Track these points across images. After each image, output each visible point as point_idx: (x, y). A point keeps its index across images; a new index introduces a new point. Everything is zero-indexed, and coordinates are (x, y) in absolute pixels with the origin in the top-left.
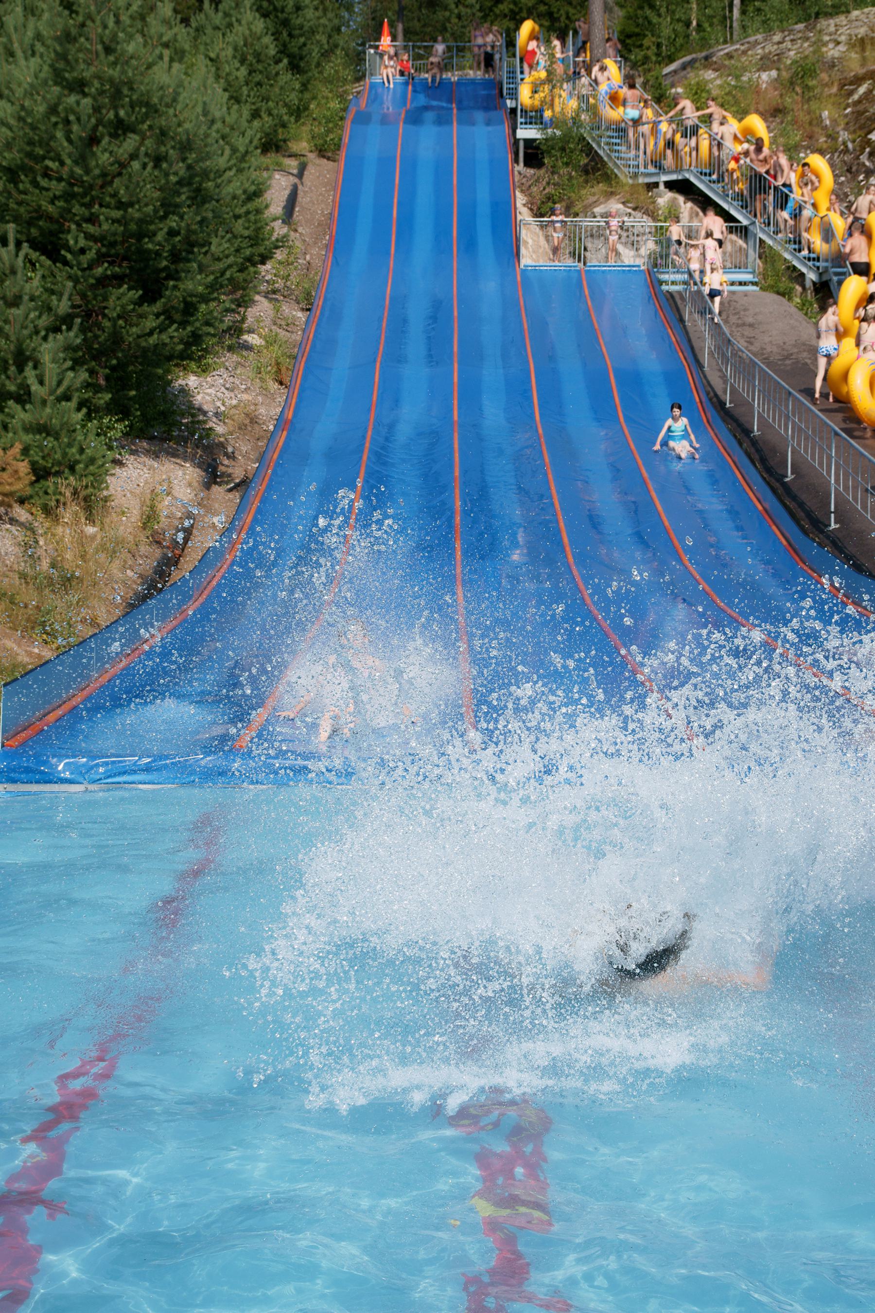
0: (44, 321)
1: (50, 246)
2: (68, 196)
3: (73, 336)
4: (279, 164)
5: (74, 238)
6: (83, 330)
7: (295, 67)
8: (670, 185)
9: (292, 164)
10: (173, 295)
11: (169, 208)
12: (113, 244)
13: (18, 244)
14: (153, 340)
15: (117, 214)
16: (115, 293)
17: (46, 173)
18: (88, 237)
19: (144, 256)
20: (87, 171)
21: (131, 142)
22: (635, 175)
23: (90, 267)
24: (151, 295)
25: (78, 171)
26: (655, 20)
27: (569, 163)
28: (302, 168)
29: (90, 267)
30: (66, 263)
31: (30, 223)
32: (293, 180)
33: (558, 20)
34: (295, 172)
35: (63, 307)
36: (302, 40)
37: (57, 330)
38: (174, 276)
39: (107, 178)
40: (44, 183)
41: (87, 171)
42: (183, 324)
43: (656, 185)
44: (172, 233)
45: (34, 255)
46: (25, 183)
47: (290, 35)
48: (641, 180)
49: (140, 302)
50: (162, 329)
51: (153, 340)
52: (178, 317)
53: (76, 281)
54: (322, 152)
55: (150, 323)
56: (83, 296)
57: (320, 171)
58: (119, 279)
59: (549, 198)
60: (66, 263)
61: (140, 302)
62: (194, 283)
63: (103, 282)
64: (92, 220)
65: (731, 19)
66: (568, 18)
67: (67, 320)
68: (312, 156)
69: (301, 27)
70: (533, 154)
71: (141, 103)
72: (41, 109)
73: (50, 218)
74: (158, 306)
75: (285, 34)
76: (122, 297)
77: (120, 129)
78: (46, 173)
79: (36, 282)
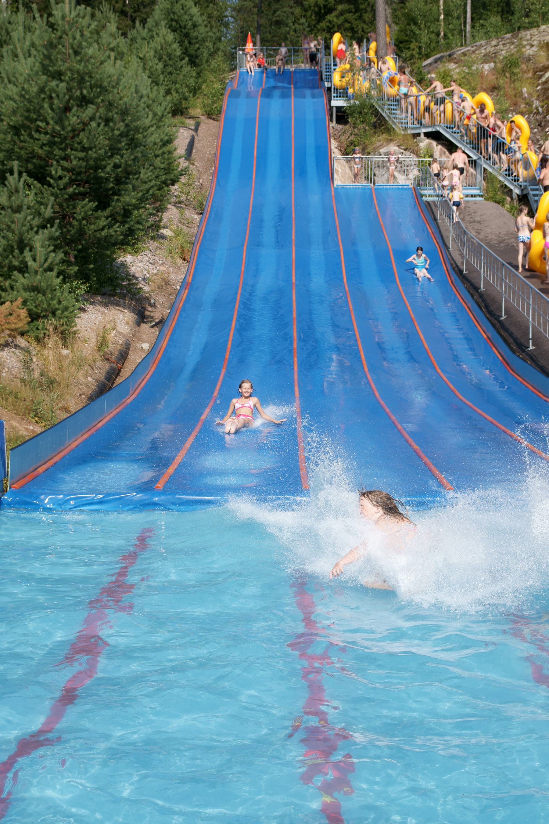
0: (37, 221)
1: (40, 175)
2: (51, 144)
4: (183, 123)
5: (55, 170)
6: (61, 227)
7: (193, 62)
10: (117, 205)
11: (114, 150)
12: (79, 173)
13: (20, 174)
15: (82, 155)
18: (64, 169)
19: (99, 181)
20: (63, 128)
21: (90, 110)
22: (406, 129)
23: (65, 188)
24: (103, 205)
25: (58, 128)
26: (418, 32)
27: (363, 121)
28: (197, 125)
29: (65, 188)
30: (50, 185)
31: (27, 161)
34: (193, 127)
35: (48, 212)
36: (197, 46)
37: (44, 227)
38: (117, 193)
39: (75, 133)
40: (36, 135)
41: (63, 128)
42: (123, 223)
43: (419, 135)
44: (116, 166)
45: (30, 180)
46: (24, 135)
47: (190, 43)
48: (409, 132)
49: (96, 209)
51: (104, 233)
52: (119, 218)
53: (56, 196)
55: (103, 222)
56: (61, 206)
57: (208, 127)
58: (83, 195)
60: (50, 185)
61: (96, 209)
62: (130, 198)
63: (73, 197)
64: (66, 158)
66: (363, 31)
67: (51, 221)
68: (203, 118)
69: (197, 38)
71: (97, 86)
73: (40, 158)
74: (107, 212)
75: (186, 42)
76: (85, 206)
77: (84, 101)
79: (31, 197)
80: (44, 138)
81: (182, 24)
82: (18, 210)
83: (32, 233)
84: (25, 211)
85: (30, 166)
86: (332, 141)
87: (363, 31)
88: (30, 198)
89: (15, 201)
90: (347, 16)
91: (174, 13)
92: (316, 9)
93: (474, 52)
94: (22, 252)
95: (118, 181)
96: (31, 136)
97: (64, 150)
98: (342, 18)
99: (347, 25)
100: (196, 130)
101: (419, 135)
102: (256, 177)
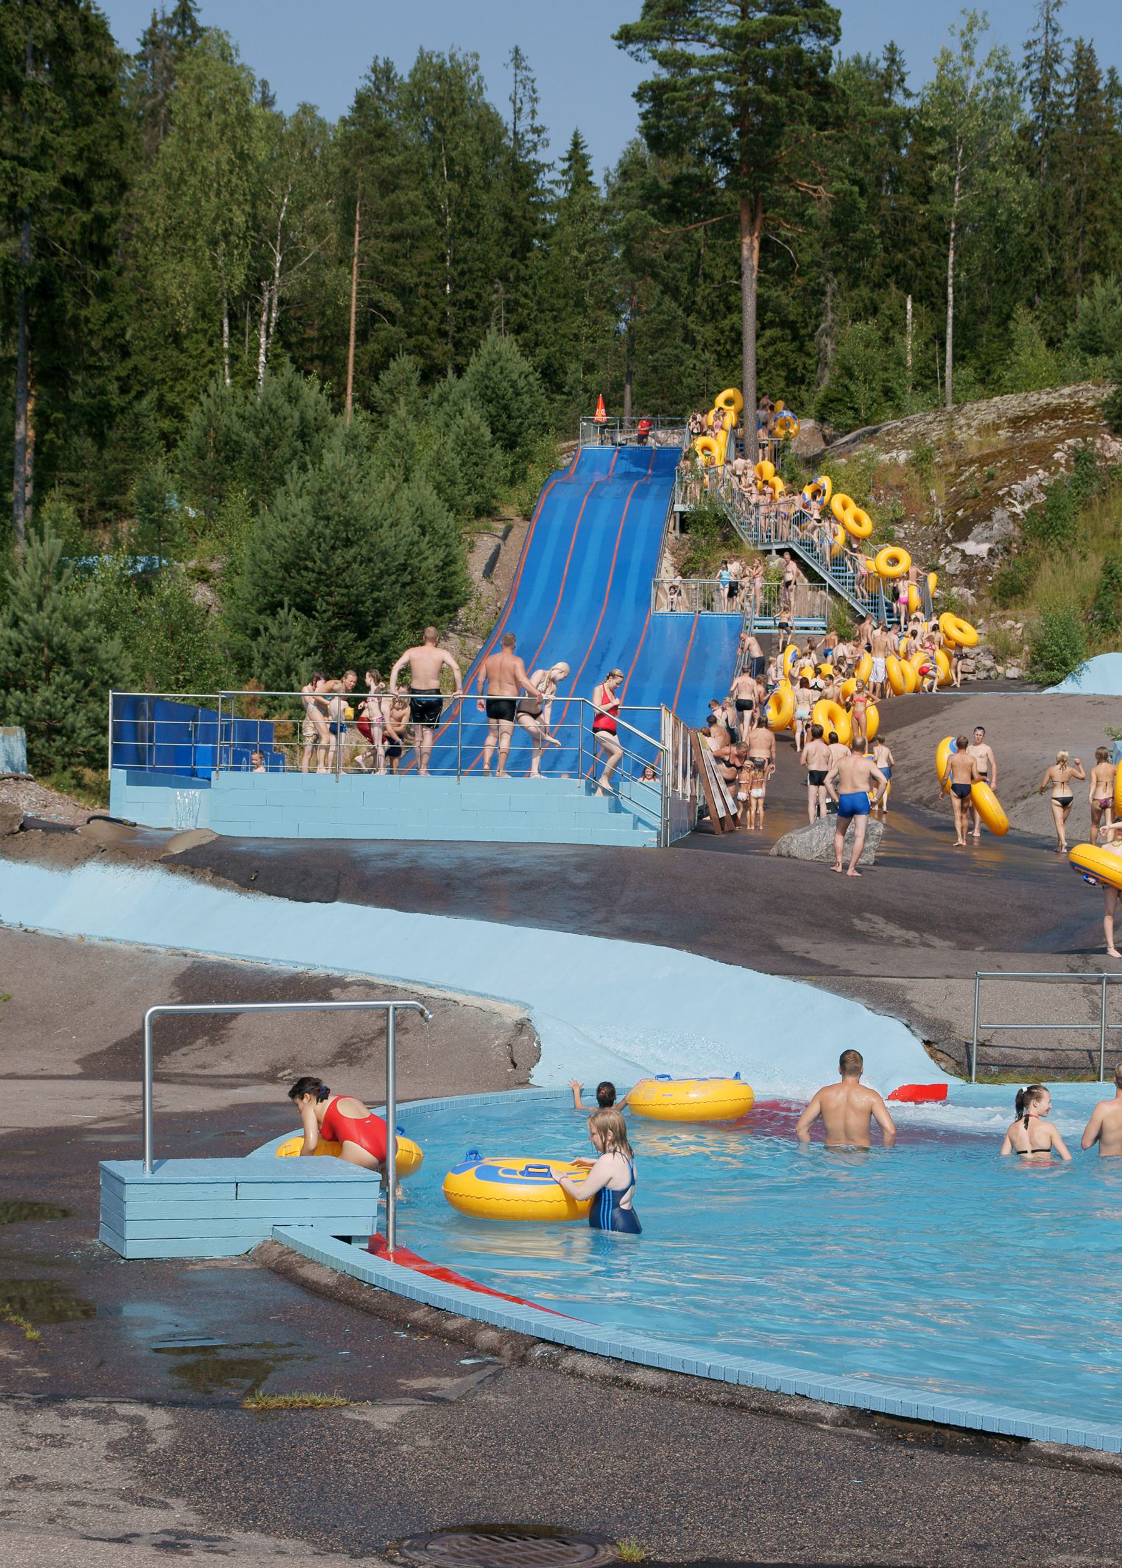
0: (302, 650)
1: (307, 609)
2: (318, 581)
3: (317, 658)
4: (488, 528)
5: (320, 605)
6: (323, 655)
7: (510, 445)
8: (780, 552)
9: (500, 527)
10: (376, 636)
11: (374, 587)
12: (342, 607)
13: (290, 607)
14: (362, 661)
15: (344, 591)
16: (341, 635)
17: (306, 568)
18: (328, 604)
19: (357, 614)
20: (329, 567)
21: (353, 551)
22: (756, 544)
23: (329, 620)
24: (362, 636)
25: (324, 567)
26: (853, 388)
27: (711, 531)
28: (509, 529)
29: (329, 620)
30: (314, 618)
31: (296, 595)
32: (497, 541)
33: (795, 370)
34: (500, 534)
35: (313, 642)
36: (519, 420)
37: (309, 655)
38: (377, 625)
39: (340, 571)
40: (304, 573)
41: (329, 567)
42: (380, 653)
43: (769, 552)
44: (376, 601)
45: (298, 614)
46: (294, 573)
47: (509, 417)
48: (760, 548)
49: (356, 640)
50: (368, 655)
51: (362, 661)
52: (378, 648)
53: (320, 628)
54: (527, 517)
55: (361, 652)
56: (324, 636)
57: (521, 529)
58: (346, 626)
59: (690, 560)
60: (314, 618)
61: (356, 640)
62: (386, 629)
63: (335, 629)
64: (330, 594)
65: (943, 377)
66: (805, 368)
67: (315, 650)
68: (518, 520)
69: (519, 410)
70: (684, 523)
71: (360, 530)
72: (304, 533)
73: (306, 592)
74: (367, 642)
75: (504, 417)
76: (349, 636)
77: (348, 543)
78: (306, 568)
79: (299, 628)
80: (312, 576)
81: (500, 393)
82: (286, 640)
83: (297, 660)
84: (293, 641)
85: (298, 600)
86: (667, 554)
87: (805, 368)
88: (297, 630)
89: (285, 632)
90: (780, 345)
91: (490, 379)
92: (733, 335)
93: (902, 429)
94: (289, 676)
95: (378, 614)
96: (298, 573)
97: (328, 586)
98: (771, 349)
99: (779, 360)
100: (505, 537)
101: (769, 552)
102: (612, 587)
